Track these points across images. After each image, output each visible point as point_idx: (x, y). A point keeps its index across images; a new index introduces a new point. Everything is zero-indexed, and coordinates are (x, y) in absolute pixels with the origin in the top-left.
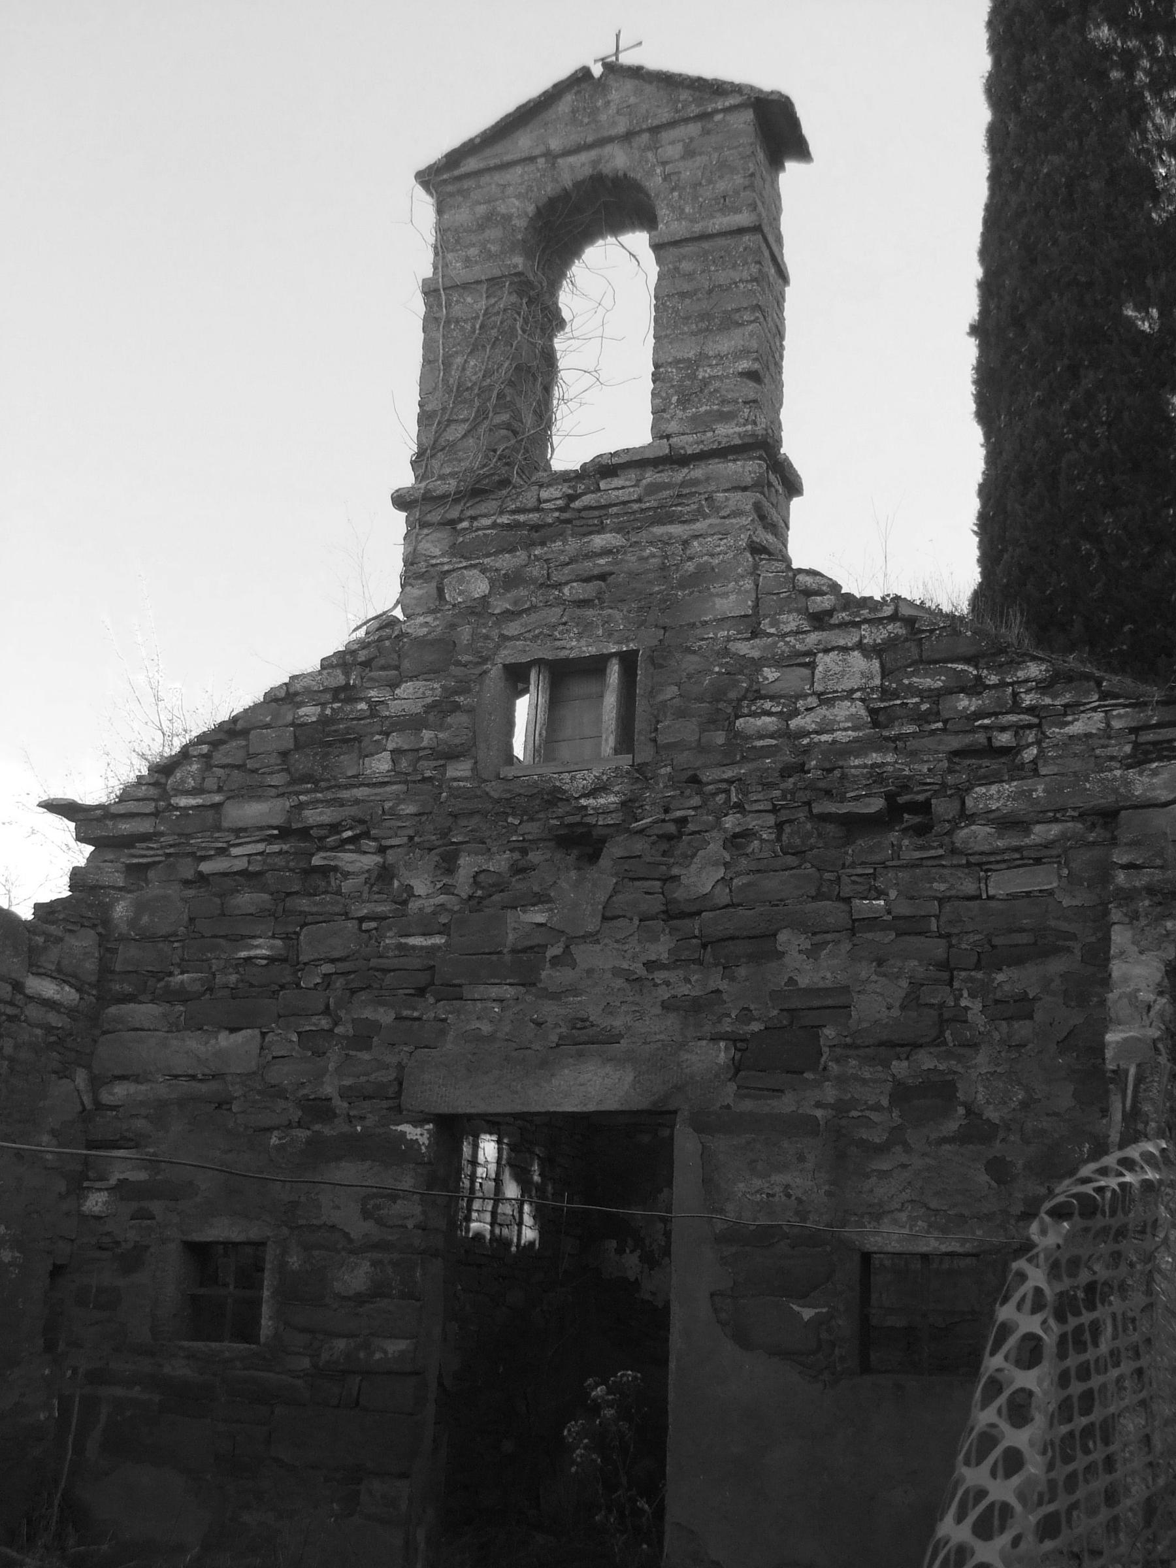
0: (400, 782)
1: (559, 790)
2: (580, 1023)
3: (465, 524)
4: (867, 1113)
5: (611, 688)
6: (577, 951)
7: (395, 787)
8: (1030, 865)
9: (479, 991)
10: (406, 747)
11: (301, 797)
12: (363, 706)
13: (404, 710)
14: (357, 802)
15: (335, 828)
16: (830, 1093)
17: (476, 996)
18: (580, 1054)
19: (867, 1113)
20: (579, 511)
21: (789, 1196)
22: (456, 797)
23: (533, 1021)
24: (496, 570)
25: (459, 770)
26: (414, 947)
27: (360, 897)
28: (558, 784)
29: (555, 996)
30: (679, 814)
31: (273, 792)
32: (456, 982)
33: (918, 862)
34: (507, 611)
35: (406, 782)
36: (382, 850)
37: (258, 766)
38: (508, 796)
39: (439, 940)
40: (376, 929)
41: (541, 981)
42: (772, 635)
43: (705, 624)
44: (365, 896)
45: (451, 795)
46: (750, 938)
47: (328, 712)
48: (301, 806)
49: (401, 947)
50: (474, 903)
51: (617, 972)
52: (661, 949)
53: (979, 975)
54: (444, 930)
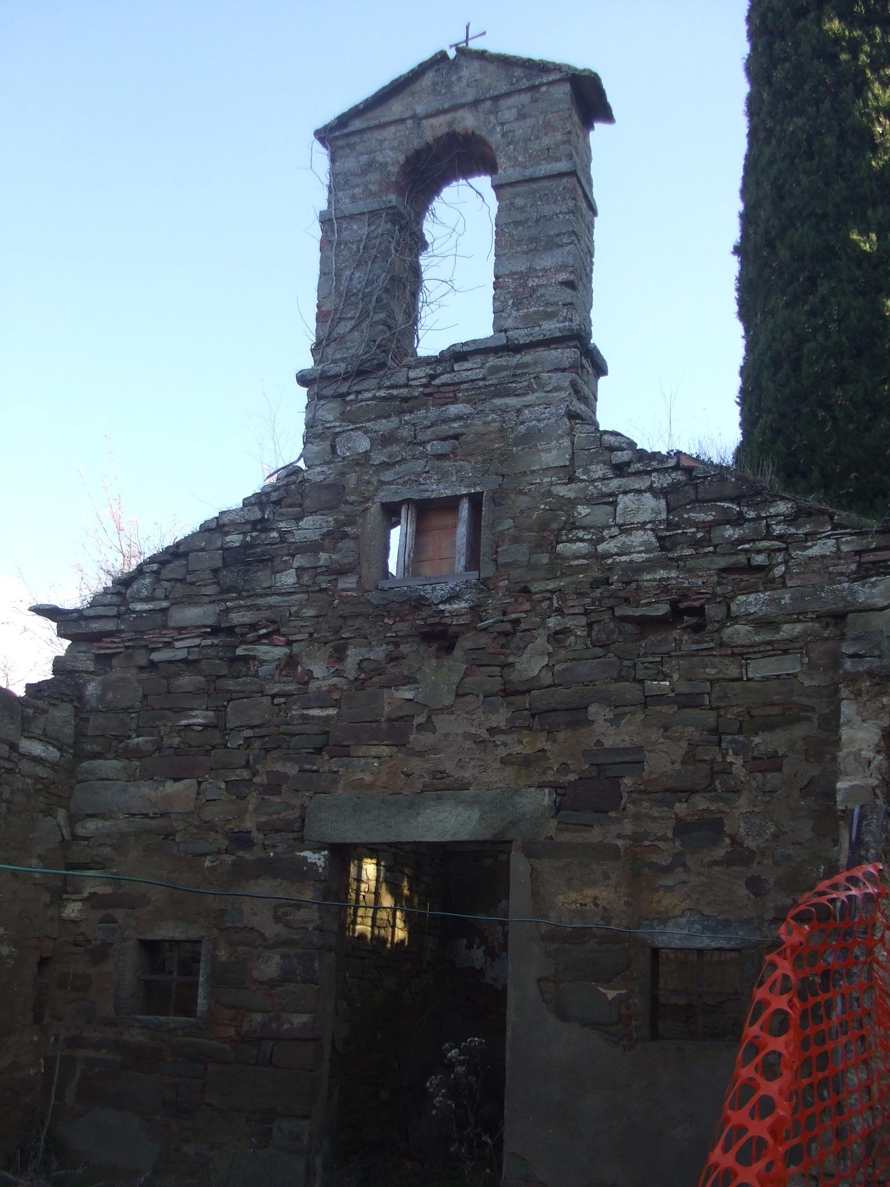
0: (302, 592)
1: (423, 598)
2: (439, 774)
3: (352, 397)
4: (657, 843)
5: (463, 520)
6: (438, 721)
7: (298, 596)
8: (780, 655)
9: (361, 751)
10: (307, 565)
11: (228, 604)
12: (275, 534)
13: (305, 537)
14: (270, 607)
15: (253, 627)
16: (628, 827)
17: (360, 754)
18: (439, 798)
19: (657, 843)
20: (438, 387)
21: (597, 905)
22: (345, 604)
23: (403, 773)
24: (376, 431)
25: (348, 583)
26: (313, 717)
27: (272, 679)
28: (422, 593)
29: (420, 754)
30: (514, 616)
31: (207, 599)
32: (345, 743)
33: (694, 653)
34: (384, 463)
35: (307, 592)
36: (289, 643)
37: (195, 580)
38: (385, 602)
39: (332, 712)
40: (284, 703)
41: (409, 743)
42: (584, 481)
43: (533, 472)
44: (277, 678)
45: (341, 602)
46: (567, 710)
47: (248, 539)
48: (228, 610)
49: (303, 717)
50: (359, 684)
51: (467, 735)
52: (500, 719)
53: (741, 738)
54: (336, 704)
